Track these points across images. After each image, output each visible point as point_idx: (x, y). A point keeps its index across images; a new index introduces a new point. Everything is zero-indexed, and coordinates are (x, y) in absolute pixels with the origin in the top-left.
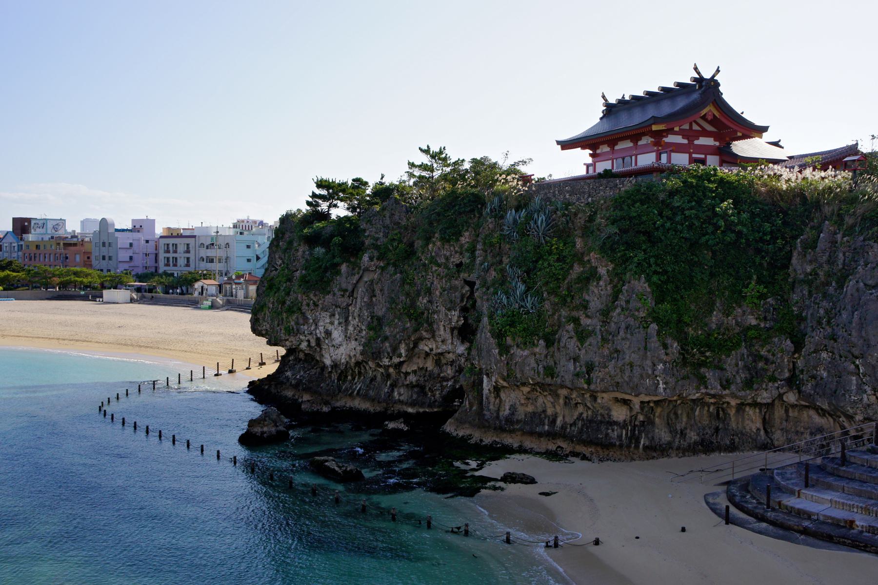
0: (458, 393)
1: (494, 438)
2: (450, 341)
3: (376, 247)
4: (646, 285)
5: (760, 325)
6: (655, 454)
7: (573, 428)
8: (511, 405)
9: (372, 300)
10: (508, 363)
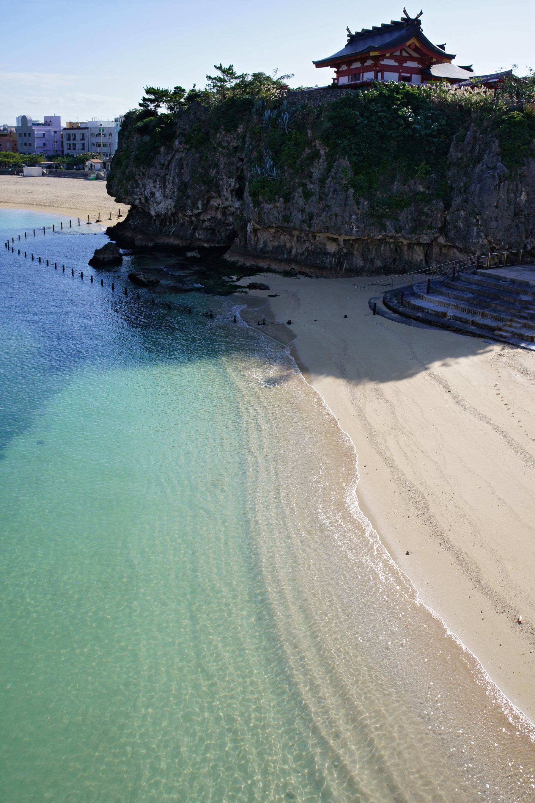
1: (252, 263)
2: (231, 199)
3: (183, 135)
4: (348, 162)
5: (425, 191)
6: (352, 274)
7: (302, 257)
8: (264, 241)
9: (181, 171)
10: (259, 213)
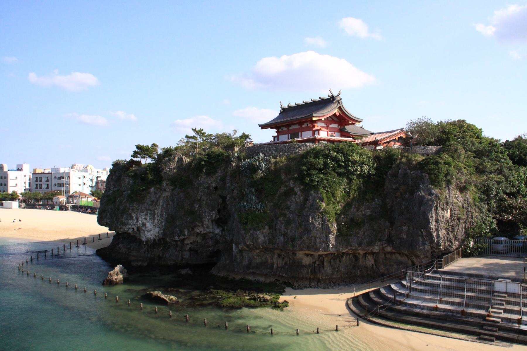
0: (217, 254)
